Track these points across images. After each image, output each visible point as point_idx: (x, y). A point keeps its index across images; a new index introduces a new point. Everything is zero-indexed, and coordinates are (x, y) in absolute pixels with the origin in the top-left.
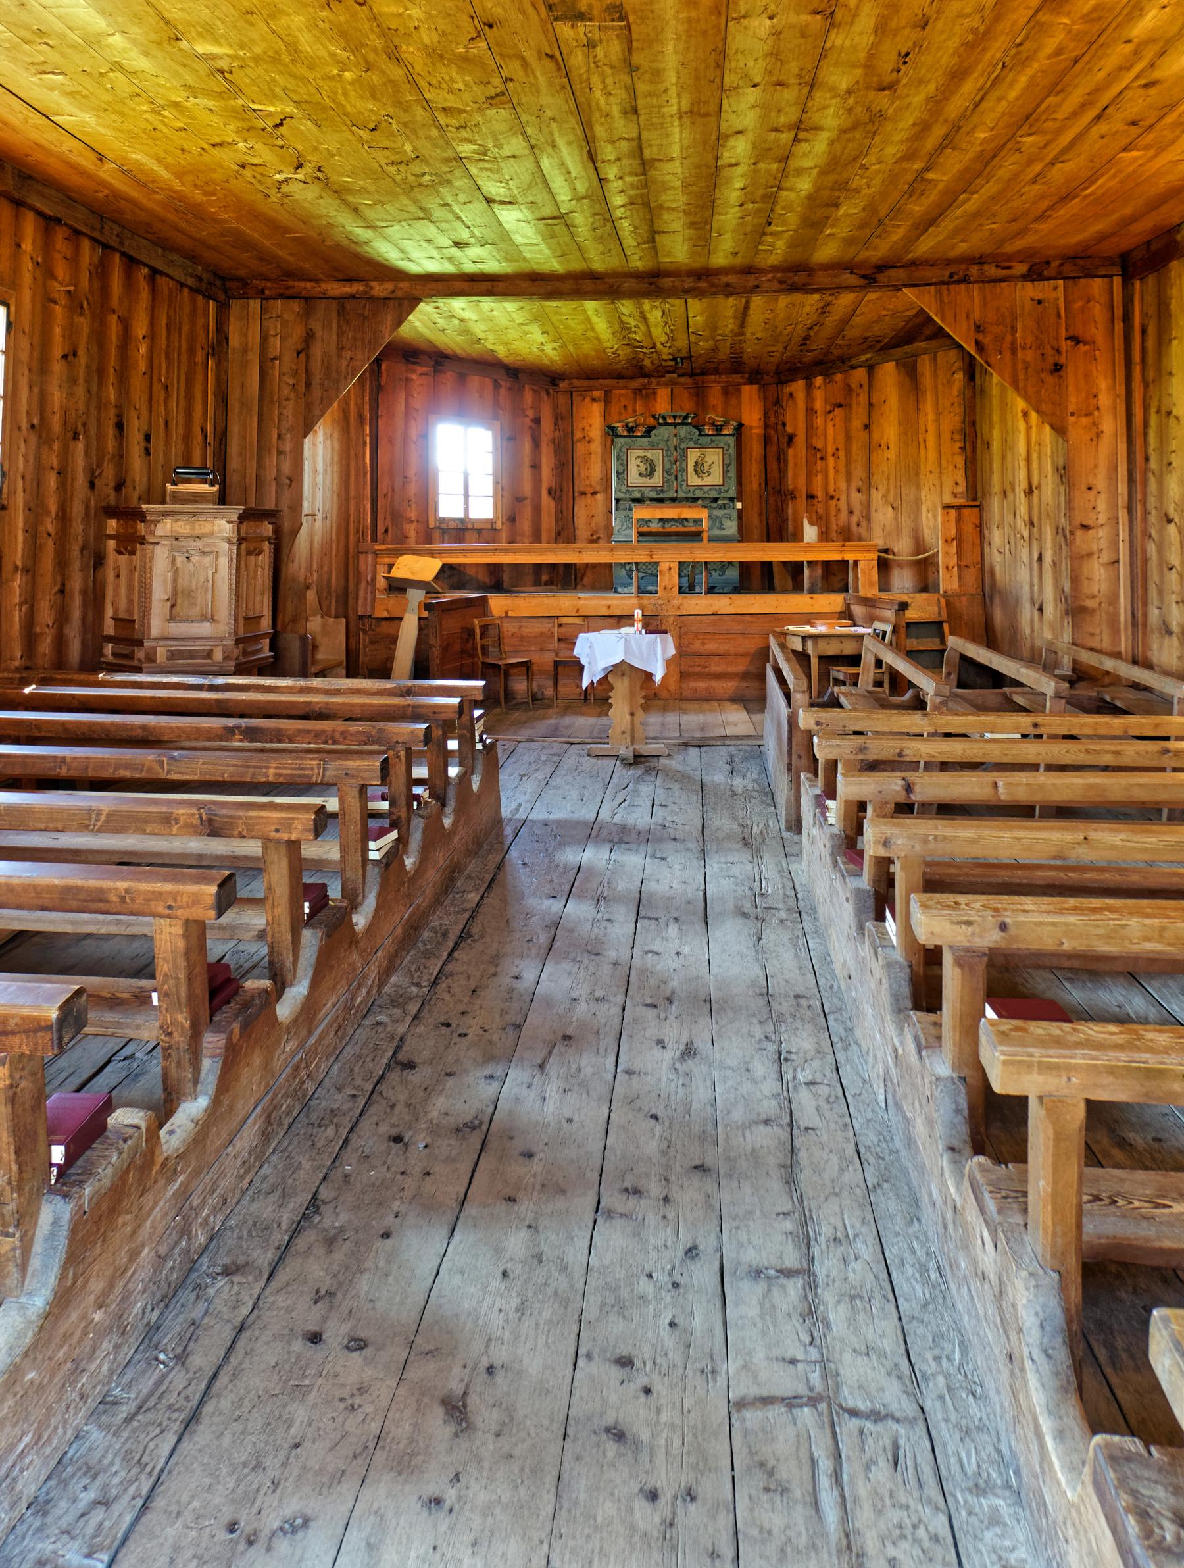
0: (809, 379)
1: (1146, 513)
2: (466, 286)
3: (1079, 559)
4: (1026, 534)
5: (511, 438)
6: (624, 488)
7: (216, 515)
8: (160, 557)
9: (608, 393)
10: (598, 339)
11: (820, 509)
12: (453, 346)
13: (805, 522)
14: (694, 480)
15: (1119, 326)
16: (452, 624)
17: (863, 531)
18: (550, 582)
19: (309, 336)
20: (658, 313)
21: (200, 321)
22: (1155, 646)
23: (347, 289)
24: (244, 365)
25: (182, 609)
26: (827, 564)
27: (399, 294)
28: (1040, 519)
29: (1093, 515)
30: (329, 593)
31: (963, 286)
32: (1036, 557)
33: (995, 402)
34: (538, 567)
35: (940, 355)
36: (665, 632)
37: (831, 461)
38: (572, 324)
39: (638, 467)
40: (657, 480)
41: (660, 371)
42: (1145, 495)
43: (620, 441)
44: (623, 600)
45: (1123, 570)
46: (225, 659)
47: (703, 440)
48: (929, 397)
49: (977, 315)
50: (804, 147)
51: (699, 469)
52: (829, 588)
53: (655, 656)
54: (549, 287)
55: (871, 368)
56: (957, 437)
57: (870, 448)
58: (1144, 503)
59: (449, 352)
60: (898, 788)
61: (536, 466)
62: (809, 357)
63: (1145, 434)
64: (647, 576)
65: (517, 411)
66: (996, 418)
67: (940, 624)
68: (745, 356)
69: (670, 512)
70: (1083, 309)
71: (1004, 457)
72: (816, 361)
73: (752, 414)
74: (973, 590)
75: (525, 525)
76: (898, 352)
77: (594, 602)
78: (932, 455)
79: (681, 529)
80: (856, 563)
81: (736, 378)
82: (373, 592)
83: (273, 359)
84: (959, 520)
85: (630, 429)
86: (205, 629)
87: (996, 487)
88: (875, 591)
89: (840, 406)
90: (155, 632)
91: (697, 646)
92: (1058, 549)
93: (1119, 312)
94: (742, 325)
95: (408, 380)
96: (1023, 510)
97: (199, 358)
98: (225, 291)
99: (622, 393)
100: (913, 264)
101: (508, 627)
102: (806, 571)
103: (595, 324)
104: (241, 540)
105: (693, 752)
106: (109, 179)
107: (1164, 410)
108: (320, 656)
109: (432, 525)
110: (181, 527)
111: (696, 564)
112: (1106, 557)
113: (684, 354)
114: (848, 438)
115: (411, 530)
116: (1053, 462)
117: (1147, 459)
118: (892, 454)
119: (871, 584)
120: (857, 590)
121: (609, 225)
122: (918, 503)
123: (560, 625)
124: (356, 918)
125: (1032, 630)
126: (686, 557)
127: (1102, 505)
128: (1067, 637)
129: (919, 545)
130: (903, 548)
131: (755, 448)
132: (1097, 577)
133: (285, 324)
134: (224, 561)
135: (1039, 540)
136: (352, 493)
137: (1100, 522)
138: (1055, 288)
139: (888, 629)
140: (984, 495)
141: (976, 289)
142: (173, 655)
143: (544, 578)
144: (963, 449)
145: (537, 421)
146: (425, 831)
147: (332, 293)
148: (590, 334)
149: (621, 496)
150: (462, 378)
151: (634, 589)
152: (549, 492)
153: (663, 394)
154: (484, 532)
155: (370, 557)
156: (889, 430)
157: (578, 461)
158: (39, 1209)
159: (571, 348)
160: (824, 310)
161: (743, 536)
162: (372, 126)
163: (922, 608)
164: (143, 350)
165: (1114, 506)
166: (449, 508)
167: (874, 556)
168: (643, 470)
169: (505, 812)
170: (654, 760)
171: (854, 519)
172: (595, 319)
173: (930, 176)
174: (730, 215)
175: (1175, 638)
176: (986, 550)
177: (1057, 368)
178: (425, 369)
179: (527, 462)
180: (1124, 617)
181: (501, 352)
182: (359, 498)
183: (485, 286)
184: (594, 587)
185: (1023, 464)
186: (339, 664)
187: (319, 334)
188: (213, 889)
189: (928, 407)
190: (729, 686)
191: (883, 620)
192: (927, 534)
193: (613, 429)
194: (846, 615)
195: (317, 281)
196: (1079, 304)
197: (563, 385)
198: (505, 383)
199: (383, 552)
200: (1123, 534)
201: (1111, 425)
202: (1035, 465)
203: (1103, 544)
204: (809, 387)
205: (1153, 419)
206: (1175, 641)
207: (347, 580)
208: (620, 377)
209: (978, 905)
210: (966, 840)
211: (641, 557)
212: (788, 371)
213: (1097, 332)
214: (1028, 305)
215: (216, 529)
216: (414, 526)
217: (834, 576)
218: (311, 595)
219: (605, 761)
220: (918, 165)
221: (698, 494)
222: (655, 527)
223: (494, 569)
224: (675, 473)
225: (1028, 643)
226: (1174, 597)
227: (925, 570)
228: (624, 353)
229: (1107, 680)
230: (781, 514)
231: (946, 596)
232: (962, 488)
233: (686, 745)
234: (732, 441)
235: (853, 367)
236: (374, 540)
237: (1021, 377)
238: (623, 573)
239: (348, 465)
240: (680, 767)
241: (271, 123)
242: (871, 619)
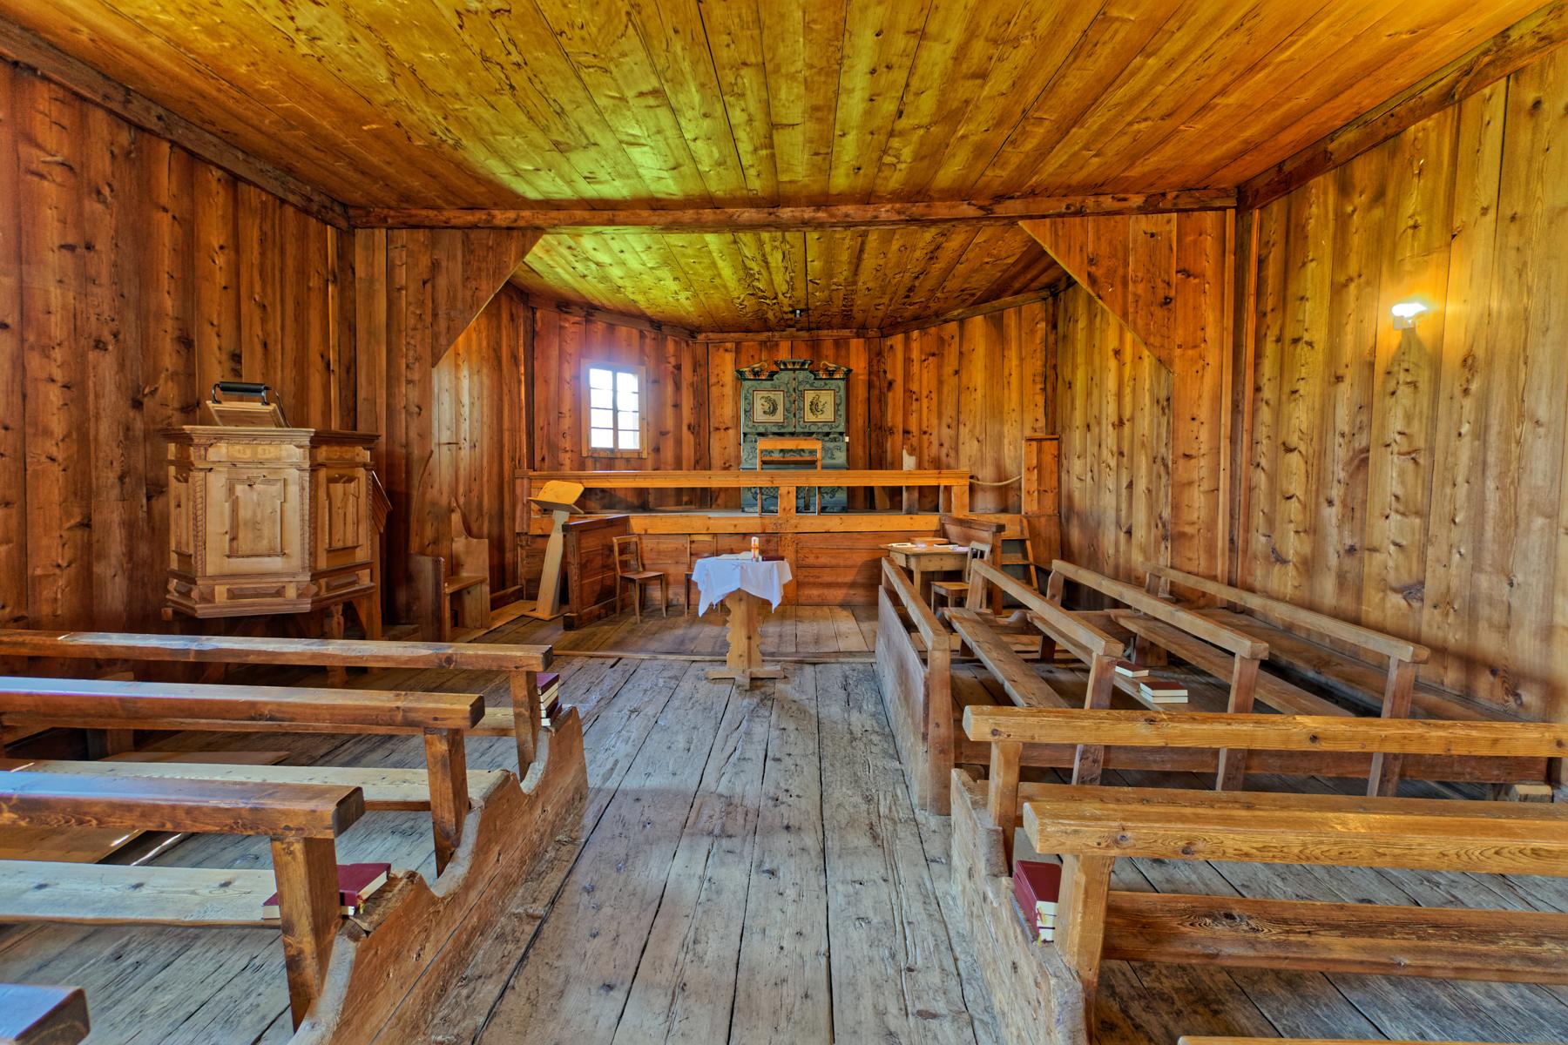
0: (907, 333)
1: (1254, 443)
2: (586, 214)
4: (1113, 463)
5: (656, 382)
7: (281, 439)
8: (217, 483)
9: (738, 344)
10: (725, 287)
11: (915, 441)
12: (596, 294)
14: (809, 417)
15: (1230, 260)
16: (591, 543)
17: (952, 461)
18: (690, 502)
19: (435, 266)
21: (313, 247)
23: (469, 218)
24: (370, 296)
25: (245, 543)
27: (521, 223)
29: (1196, 446)
30: (481, 514)
31: (1078, 220)
32: (1124, 484)
34: (679, 491)
35: (1024, 308)
36: (782, 559)
37: (925, 402)
39: (763, 405)
40: (779, 417)
41: (784, 324)
43: (747, 384)
44: (749, 519)
45: (1223, 497)
46: (299, 596)
47: (818, 384)
48: (1014, 345)
49: (1090, 248)
51: (814, 407)
52: (922, 509)
53: (772, 581)
54: (670, 216)
55: (962, 322)
56: (1038, 379)
57: (961, 390)
59: (596, 302)
62: (910, 311)
63: (1257, 366)
64: (769, 497)
65: (661, 358)
66: (1080, 359)
67: (1023, 542)
68: (855, 309)
69: (789, 444)
70: (1195, 242)
71: (1089, 394)
72: (915, 314)
73: (858, 362)
74: (1050, 512)
75: (668, 453)
76: (987, 306)
78: (1015, 396)
79: (798, 458)
80: (948, 489)
81: (846, 332)
82: (529, 513)
83: (399, 290)
84: (1040, 451)
85: (756, 374)
86: (275, 564)
87: (1078, 419)
88: (967, 512)
90: (210, 570)
91: (811, 560)
93: (1230, 245)
94: (856, 273)
95: (561, 327)
96: (1110, 440)
97: (314, 282)
98: (348, 219)
99: (751, 342)
100: (1033, 193)
101: (648, 544)
102: (905, 495)
104: (315, 468)
105: (808, 670)
106: (155, 55)
107: (1288, 336)
108: (464, 574)
110: (241, 452)
111: (810, 489)
112: (1205, 486)
114: (940, 382)
115: (566, 459)
117: (1258, 389)
118: (979, 395)
119: (963, 506)
120: (949, 509)
122: (1001, 436)
123: (692, 542)
124: (522, 785)
125: (1117, 550)
126: (802, 483)
127: (1204, 435)
128: (1164, 559)
129: (1001, 474)
130: (986, 475)
131: (861, 392)
132: (1197, 505)
133: (410, 254)
134: (294, 490)
135: (1130, 469)
136: (506, 425)
138: (1169, 221)
139: (987, 549)
141: (1090, 223)
143: (685, 499)
144: (1044, 389)
145: (678, 367)
146: (357, 965)
147: (454, 222)
148: (717, 281)
151: (758, 509)
153: (785, 346)
154: (632, 461)
155: (526, 481)
156: (977, 373)
157: (714, 401)
158: (331, 943)
159: (702, 297)
161: (851, 464)
164: (220, 260)
165: (1215, 436)
166: (600, 439)
167: (967, 482)
169: (594, 781)
170: (769, 683)
171: (944, 451)
172: (720, 263)
174: (849, 150)
175: (1291, 567)
176: (1064, 476)
177: (1167, 301)
178: (577, 319)
179: (670, 402)
180: (1221, 542)
182: (514, 431)
184: (727, 507)
185: (1112, 399)
186: (482, 582)
187: (444, 264)
188: (332, 808)
189: (1013, 354)
190: (839, 594)
191: (982, 541)
192: (1009, 465)
193: (741, 373)
194: (942, 533)
195: (439, 209)
196: (1190, 238)
197: (701, 337)
198: (650, 334)
199: (536, 478)
200: (1224, 462)
201: (1216, 355)
202: (1128, 399)
203: (1204, 473)
204: (907, 340)
205: (1270, 348)
207: (502, 502)
208: (748, 331)
211: (763, 482)
212: (891, 325)
213: (1208, 266)
214: (1141, 236)
215: (284, 453)
216: (568, 455)
217: (929, 499)
218: (456, 518)
219: (717, 687)
221: (814, 429)
222: (777, 456)
223: (642, 492)
224: (794, 410)
225: (1111, 561)
227: (1006, 497)
228: (750, 303)
229: (1202, 602)
230: (881, 445)
231: (1027, 517)
232: (1042, 423)
233: (801, 662)
234: (842, 384)
235: (946, 321)
236: (532, 466)
237: (1131, 310)
238: (750, 495)
239: (501, 400)
240: (796, 696)
242: (967, 540)
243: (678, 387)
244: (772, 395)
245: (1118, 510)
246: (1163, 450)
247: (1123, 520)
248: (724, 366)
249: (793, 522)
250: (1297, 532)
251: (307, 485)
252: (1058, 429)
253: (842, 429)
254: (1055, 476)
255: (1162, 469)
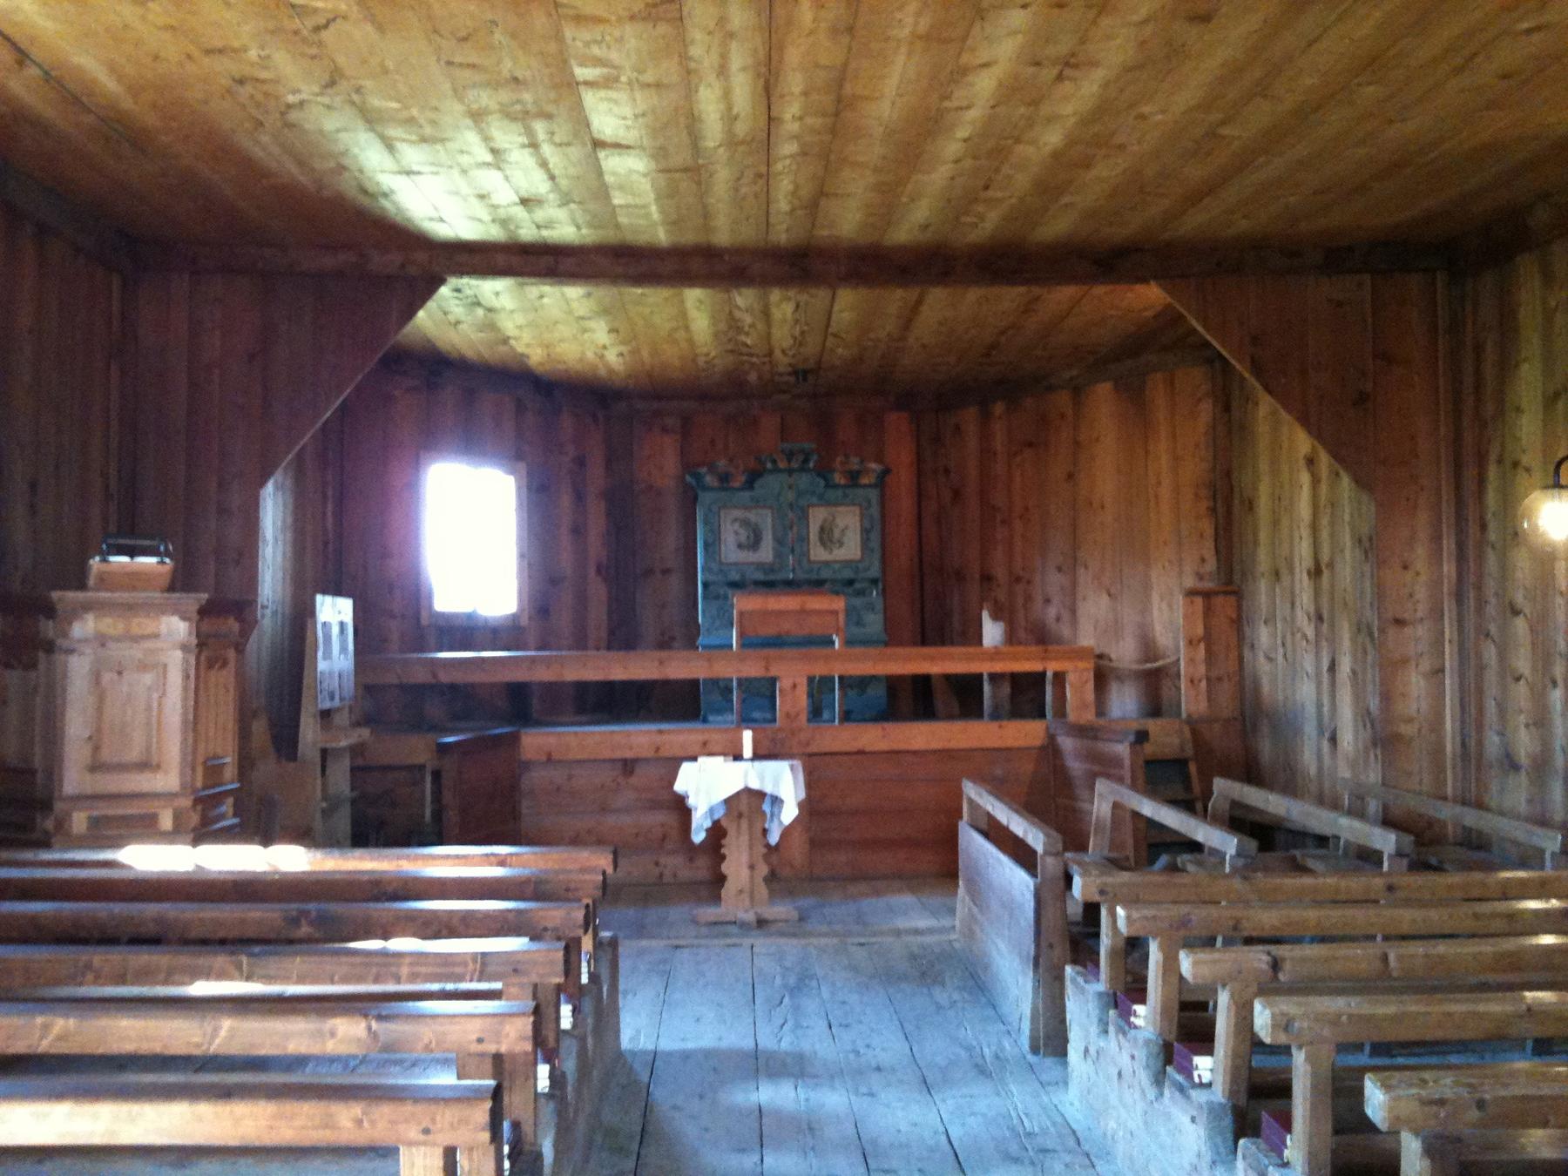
2: (515, 260)
3: (1391, 667)
6: (715, 566)
7: (163, 609)
10: (690, 341)
11: (1001, 595)
13: (985, 615)
14: (818, 553)
20: (788, 308)
22: (1494, 787)
23: (328, 262)
26: (1015, 678)
27: (412, 270)
28: (1332, 610)
33: (1263, 443)
38: (657, 319)
40: (766, 553)
42: (1480, 576)
50: (1067, 87)
52: (1017, 713)
55: (1077, 391)
56: (1204, 492)
58: (1479, 588)
60: (1265, 967)
61: (578, 531)
66: (1264, 466)
71: (1276, 523)
73: (902, 455)
75: (564, 620)
77: (681, 738)
80: (1060, 678)
84: (1208, 612)
89: (1030, 445)
92: (1359, 654)
96: (1305, 598)
102: (987, 688)
103: (694, 319)
104: (201, 645)
109: (424, 621)
110: (110, 625)
112: (1426, 665)
113: (811, 364)
116: (1352, 530)
120: (1061, 712)
121: (761, 182)
127: (1421, 593)
130: (1125, 653)
134: (175, 679)
137: (1420, 614)
140: (1244, 574)
142: (95, 823)
149: (711, 578)
150: (469, 397)
152: (599, 571)
154: (495, 634)
159: (645, 354)
160: (1028, 308)
162: (463, 33)
163: (1167, 737)
168: (743, 539)
173: (1225, 131)
176: (1247, 653)
177: (1362, 399)
181: (536, 357)
183: (547, 260)
185: (1305, 532)
189: (1161, 447)
202: (1325, 534)
204: (986, 417)
206: (1523, 778)
209: (1448, 1081)
210: (1386, 1018)
211: (753, 669)
217: (1026, 694)
220: (1216, 116)
221: (825, 574)
224: (791, 539)
226: (1522, 718)
228: (723, 363)
231: (1190, 721)
232: (1211, 565)
234: (873, 494)
241: (310, 23)
243: (579, 497)
244: (752, 516)
245: (1319, 706)
246: (1368, 613)
247: (1326, 720)
248: (661, 462)
249: (803, 736)
250: (1527, 726)
251: (192, 673)
252: (1237, 577)
253: (875, 571)
254: (1234, 654)
255: (1368, 640)
